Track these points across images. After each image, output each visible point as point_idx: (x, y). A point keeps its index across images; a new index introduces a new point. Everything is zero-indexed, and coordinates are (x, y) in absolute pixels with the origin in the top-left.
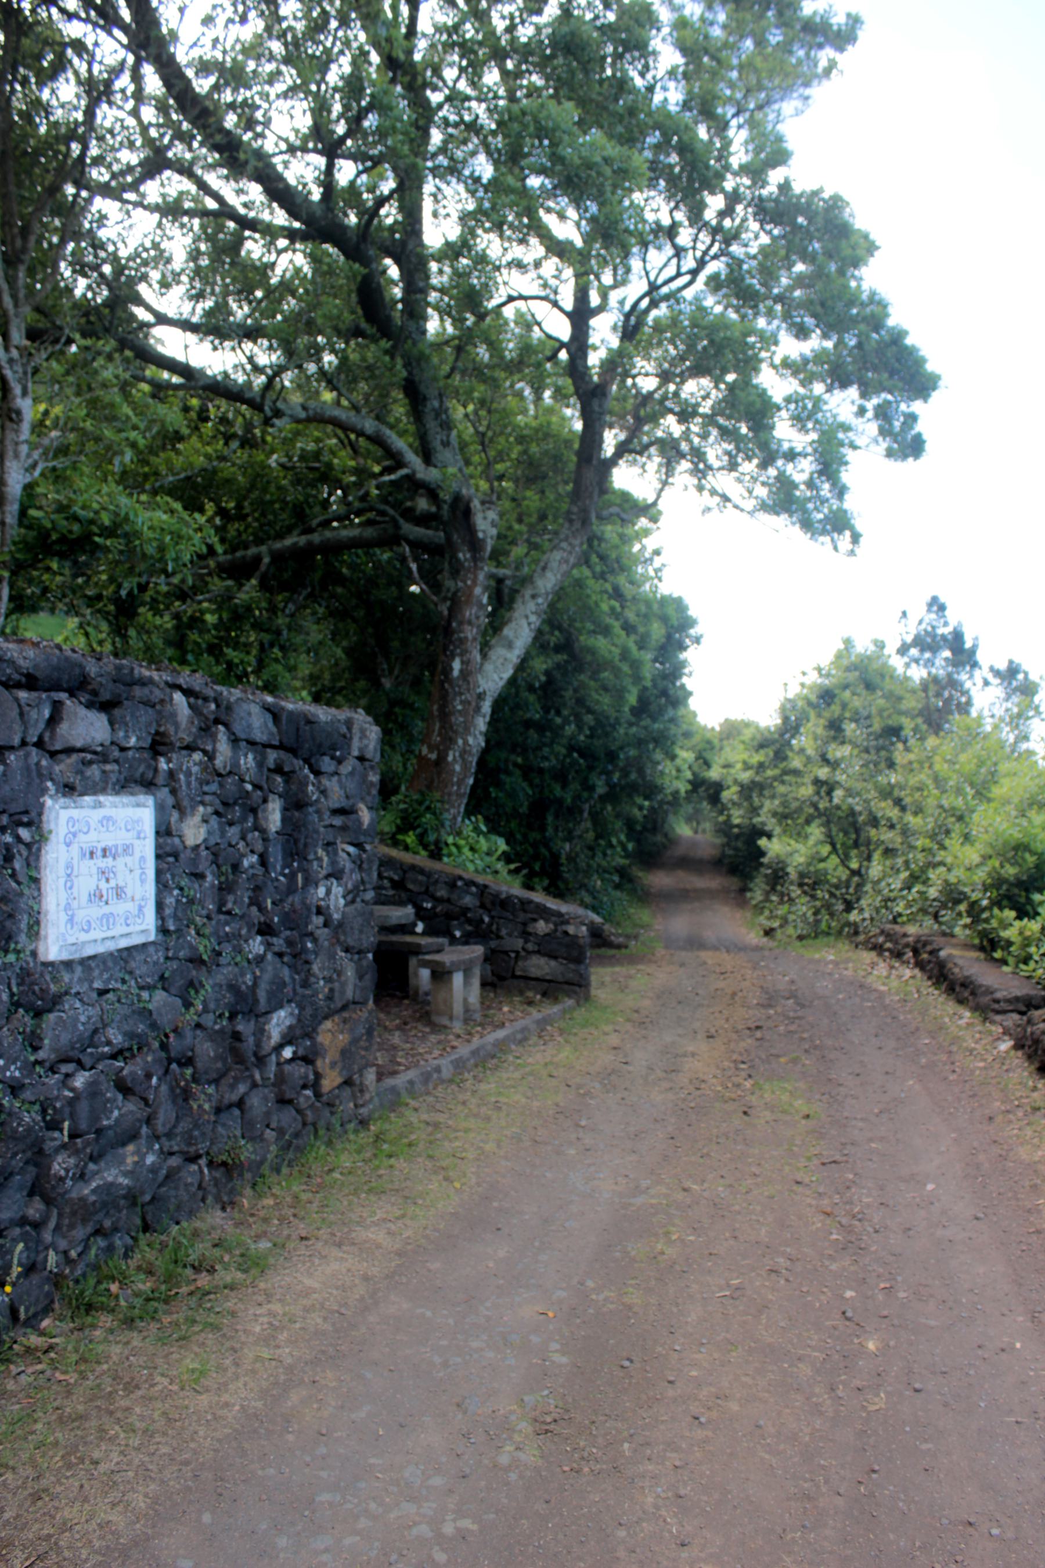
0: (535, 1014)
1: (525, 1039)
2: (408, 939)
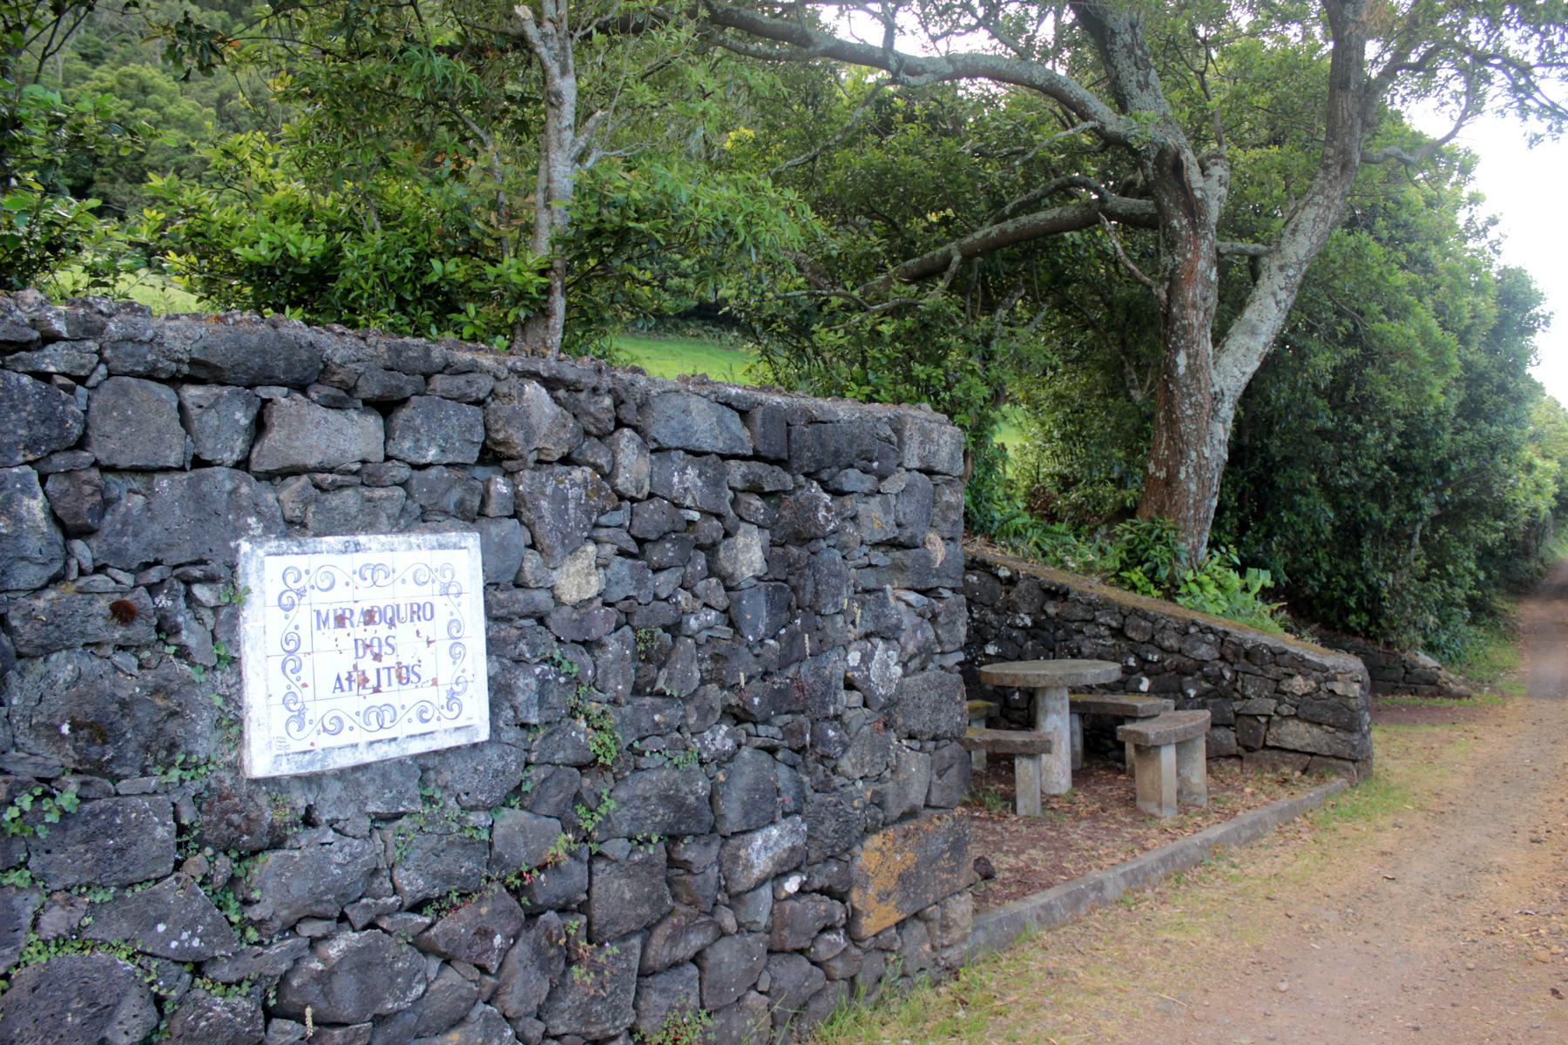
0: (1284, 799)
1: (1256, 836)
2: (1125, 700)
